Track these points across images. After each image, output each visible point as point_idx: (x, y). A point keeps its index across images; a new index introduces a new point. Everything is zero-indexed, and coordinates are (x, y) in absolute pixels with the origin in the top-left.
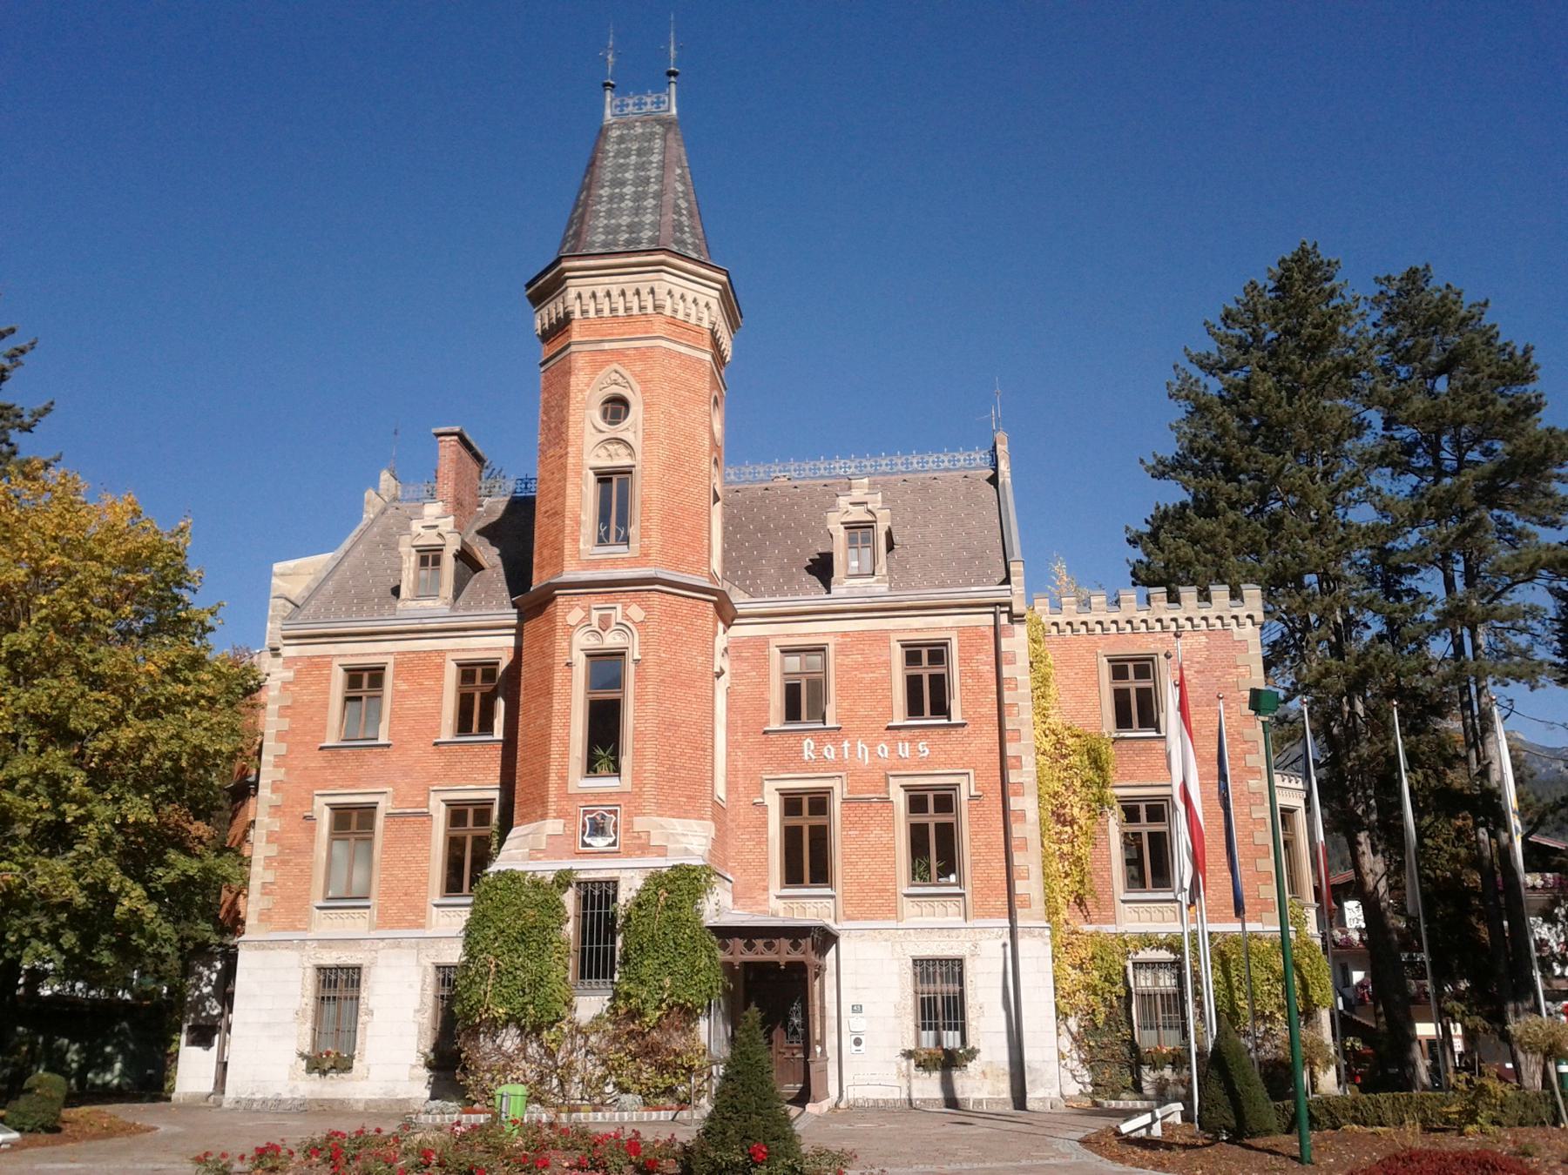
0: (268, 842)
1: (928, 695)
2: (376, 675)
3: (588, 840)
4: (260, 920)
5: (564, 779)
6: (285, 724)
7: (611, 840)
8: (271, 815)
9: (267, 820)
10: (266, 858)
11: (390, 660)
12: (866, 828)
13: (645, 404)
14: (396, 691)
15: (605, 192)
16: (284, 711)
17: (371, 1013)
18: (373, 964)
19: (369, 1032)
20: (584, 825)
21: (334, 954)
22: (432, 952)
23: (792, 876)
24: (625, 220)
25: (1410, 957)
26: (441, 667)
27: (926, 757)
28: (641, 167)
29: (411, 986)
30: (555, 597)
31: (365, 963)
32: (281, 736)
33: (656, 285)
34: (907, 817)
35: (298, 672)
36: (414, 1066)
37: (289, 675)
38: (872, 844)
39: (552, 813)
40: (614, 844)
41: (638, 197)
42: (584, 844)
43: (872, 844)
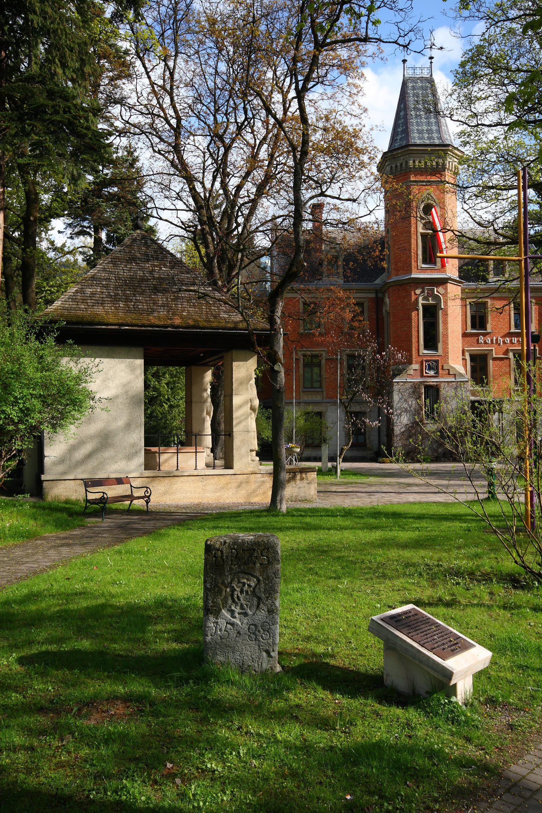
18: (326, 411)
24: (425, 128)
25: (438, 448)
30: (447, 283)
39: (414, 362)
42: (426, 373)
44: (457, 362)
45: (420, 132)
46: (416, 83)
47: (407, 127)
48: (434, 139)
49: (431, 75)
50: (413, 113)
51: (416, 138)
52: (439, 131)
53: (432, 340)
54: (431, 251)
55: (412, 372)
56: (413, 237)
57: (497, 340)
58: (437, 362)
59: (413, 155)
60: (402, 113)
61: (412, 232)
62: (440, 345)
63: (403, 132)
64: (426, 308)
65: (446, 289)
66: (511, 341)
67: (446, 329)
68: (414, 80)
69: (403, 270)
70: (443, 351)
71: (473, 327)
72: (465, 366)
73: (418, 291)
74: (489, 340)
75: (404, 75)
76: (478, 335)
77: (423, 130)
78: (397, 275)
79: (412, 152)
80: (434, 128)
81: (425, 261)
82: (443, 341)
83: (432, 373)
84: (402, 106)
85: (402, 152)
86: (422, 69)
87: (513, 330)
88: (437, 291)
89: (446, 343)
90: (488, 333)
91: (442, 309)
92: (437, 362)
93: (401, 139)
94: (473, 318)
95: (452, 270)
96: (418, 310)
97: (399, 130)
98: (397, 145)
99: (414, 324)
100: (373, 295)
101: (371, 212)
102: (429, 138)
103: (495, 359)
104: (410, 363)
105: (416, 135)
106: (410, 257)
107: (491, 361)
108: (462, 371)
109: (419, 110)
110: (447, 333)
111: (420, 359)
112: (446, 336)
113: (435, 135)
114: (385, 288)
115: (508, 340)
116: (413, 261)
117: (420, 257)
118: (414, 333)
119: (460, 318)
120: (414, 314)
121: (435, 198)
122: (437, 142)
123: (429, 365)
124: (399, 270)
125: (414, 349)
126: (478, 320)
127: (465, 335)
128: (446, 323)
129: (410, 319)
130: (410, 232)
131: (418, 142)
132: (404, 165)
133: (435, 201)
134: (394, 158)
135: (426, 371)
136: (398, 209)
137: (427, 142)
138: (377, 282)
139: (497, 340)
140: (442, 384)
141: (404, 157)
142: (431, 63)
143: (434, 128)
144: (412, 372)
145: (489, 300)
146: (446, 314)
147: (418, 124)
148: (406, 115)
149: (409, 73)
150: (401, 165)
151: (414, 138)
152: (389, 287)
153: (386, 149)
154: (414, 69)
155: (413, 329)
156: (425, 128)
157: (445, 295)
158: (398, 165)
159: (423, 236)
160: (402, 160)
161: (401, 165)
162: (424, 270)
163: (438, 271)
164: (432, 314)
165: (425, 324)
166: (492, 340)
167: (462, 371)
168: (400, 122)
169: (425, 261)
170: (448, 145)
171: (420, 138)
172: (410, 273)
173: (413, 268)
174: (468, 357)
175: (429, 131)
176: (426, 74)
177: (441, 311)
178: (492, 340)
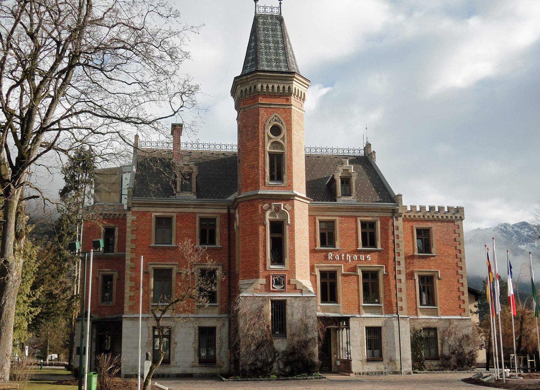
0: (130, 281)
1: (369, 239)
2: (169, 220)
3: (274, 286)
4: (129, 310)
5: (265, 265)
6: (134, 237)
7: (282, 287)
8: (130, 271)
9: (130, 273)
10: (130, 287)
11: (175, 215)
12: (350, 283)
13: (287, 130)
14: (177, 227)
15: (262, 44)
16: (133, 232)
17: (176, 343)
19: (176, 350)
20: (273, 281)
21: (208, 322)
22: (198, 322)
23: (324, 299)
24: (273, 57)
26: (195, 218)
27: (371, 261)
28: (274, 36)
29: (191, 334)
31: (173, 326)
32: (133, 241)
33: (285, 85)
34: (320, 280)
35: (137, 217)
36: (193, 362)
37: (135, 218)
38: (349, 290)
40: (284, 288)
41: (276, 49)
43: (349, 290)
44: (304, 277)
45: (269, 61)
46: (266, 19)
47: (256, 56)
48: (281, 67)
49: (281, 14)
50: (262, 44)
51: (264, 66)
52: (286, 61)
53: (279, 253)
54: (279, 168)
55: (259, 287)
56: (261, 155)
57: (345, 257)
58: (284, 277)
59: (261, 80)
60: (253, 44)
61: (260, 151)
62: (287, 260)
63: (253, 60)
64: (272, 223)
65: (293, 206)
66: (359, 258)
67: (293, 244)
68: (265, 17)
69: (252, 186)
70: (290, 266)
71: (323, 244)
72: (314, 283)
73: (266, 205)
74: (337, 257)
75: (256, 12)
76: (328, 251)
77: (271, 59)
78: (246, 191)
79: (259, 78)
80: (282, 58)
81: (272, 178)
82: (290, 256)
83: (278, 288)
84: (253, 38)
85: (251, 77)
86: (272, 8)
87: (360, 248)
88: (284, 208)
89: (293, 259)
90: (337, 250)
91: (288, 224)
92: (284, 277)
93: (251, 66)
94: (322, 236)
95: (299, 187)
96: (265, 226)
97: (250, 58)
98: (247, 71)
99: (261, 239)
100: (225, 211)
101: (175, 113)
102: (276, 66)
103: (343, 275)
104: (258, 277)
105: (265, 63)
106: (258, 174)
107: (340, 277)
108: (311, 289)
109: (269, 42)
110: (294, 248)
111: (266, 274)
112: (293, 251)
113: (282, 64)
114: (235, 204)
115: (355, 257)
116: (260, 178)
117: (268, 174)
118: (261, 248)
119: (307, 234)
120: (261, 228)
121: (282, 120)
122: (284, 70)
123: (276, 280)
124: (248, 187)
125: (261, 264)
126: (326, 237)
127: (313, 251)
128: (292, 238)
129: (257, 233)
130: (258, 151)
131: (266, 69)
132: (253, 89)
133: (281, 123)
134: (246, 82)
135: (272, 286)
136: (248, 127)
137: (275, 69)
138: (229, 198)
139: (345, 257)
140: (288, 299)
141: (253, 82)
142: (280, 3)
143: (282, 58)
144: (259, 287)
145: (337, 219)
146: (292, 230)
147: (266, 54)
148: (256, 45)
149: (261, 11)
150: (251, 88)
151: (263, 66)
152: (238, 203)
153: (239, 74)
154: (265, 7)
155: (260, 244)
156: (273, 57)
157: (292, 211)
158: (248, 89)
159: (271, 155)
160: (251, 84)
161: (251, 88)
162: (272, 187)
163: (285, 188)
164: (278, 228)
165: (272, 239)
166: (340, 257)
167: (311, 289)
168: (251, 51)
169: (272, 178)
170: (294, 73)
171: (268, 66)
172: (257, 188)
173: (261, 185)
174: (318, 274)
175: (277, 61)
176: (276, 12)
177: (287, 227)
178: (340, 257)
